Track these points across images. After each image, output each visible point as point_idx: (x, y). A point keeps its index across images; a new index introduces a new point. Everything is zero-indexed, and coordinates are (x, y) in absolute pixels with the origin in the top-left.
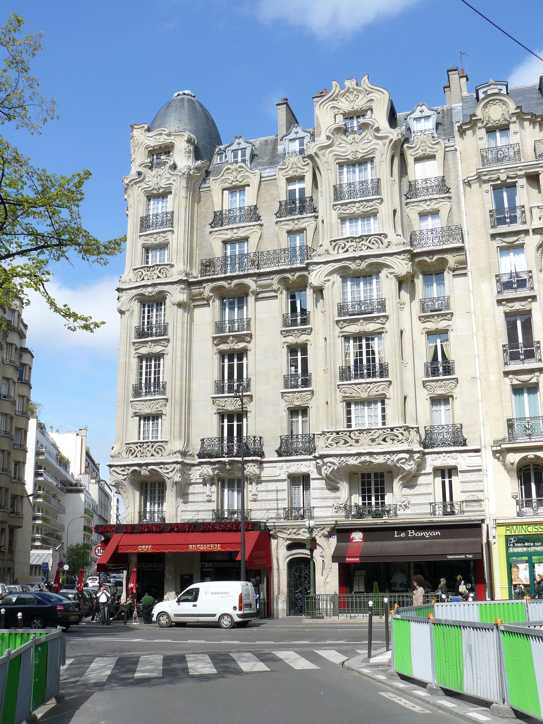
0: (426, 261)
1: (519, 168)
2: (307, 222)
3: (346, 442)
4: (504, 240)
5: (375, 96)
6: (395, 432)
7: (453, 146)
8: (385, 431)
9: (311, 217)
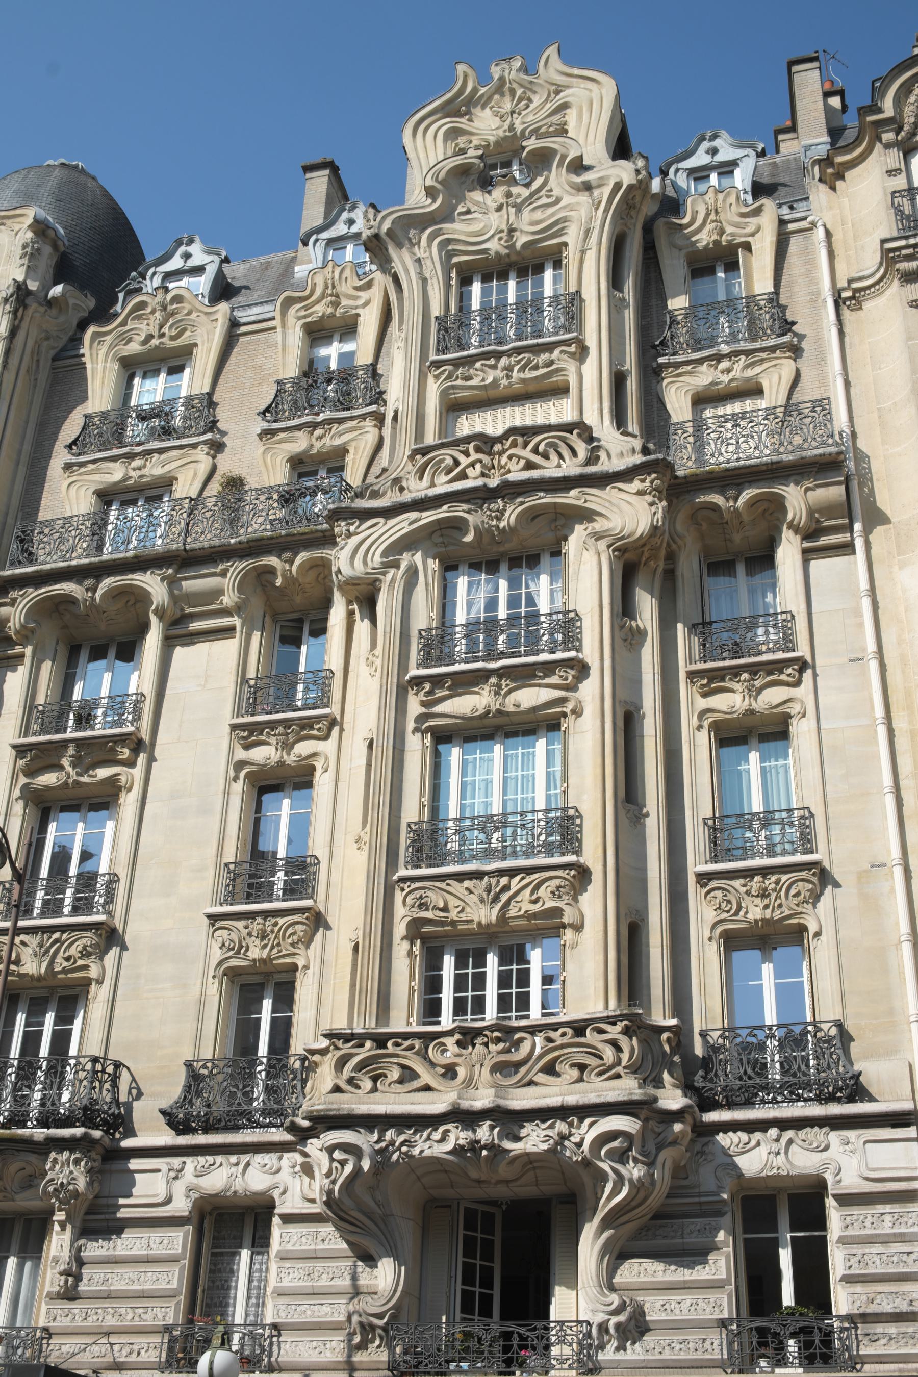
0: (715, 508)
2: (351, 430)
3: (408, 1074)
5: (577, 93)
6: (590, 1037)
7: (805, 218)
8: (552, 1034)
9: (363, 417)
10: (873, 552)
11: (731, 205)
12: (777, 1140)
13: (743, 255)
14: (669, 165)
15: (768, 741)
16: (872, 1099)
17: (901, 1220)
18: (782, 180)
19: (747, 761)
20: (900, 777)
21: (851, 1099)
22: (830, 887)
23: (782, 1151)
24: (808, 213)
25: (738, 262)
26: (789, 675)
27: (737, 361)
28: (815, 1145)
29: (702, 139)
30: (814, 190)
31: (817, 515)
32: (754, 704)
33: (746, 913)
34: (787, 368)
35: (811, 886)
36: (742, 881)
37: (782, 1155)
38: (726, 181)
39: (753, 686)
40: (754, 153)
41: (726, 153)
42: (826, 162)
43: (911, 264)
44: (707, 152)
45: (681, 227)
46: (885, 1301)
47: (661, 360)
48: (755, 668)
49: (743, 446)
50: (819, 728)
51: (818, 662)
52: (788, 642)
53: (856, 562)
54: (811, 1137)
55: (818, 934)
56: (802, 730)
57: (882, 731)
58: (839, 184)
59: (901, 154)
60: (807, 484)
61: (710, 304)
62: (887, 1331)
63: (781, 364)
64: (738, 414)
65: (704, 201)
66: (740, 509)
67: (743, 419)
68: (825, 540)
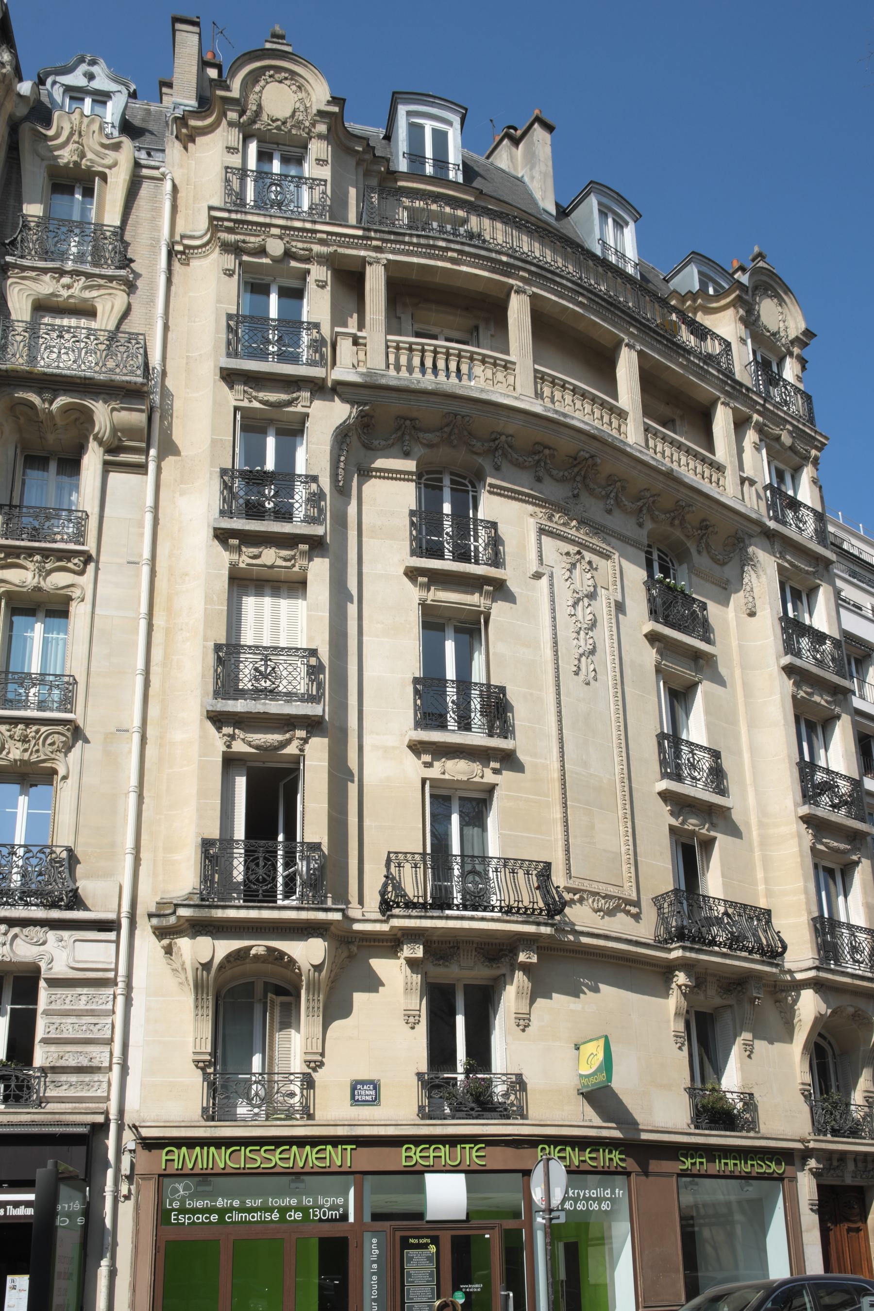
0: (31, 405)
1: (319, 235)
4: (261, 395)
7: (158, 168)
10: (163, 476)
11: (94, 132)
12: (5, 934)
13: (99, 185)
14: (48, 74)
15: (54, 617)
16: (87, 909)
17: (93, 1000)
18: (150, 128)
19: (33, 629)
20: (152, 664)
21: (69, 907)
22: (80, 742)
23: (8, 943)
24: (162, 164)
25: (93, 189)
26: (75, 564)
27: (78, 281)
28: (35, 940)
29: (82, 60)
30: (170, 144)
31: (119, 434)
32: (42, 583)
33: (8, 753)
34: (120, 299)
35: (64, 739)
36: (7, 727)
37: (8, 946)
38: (98, 109)
39: (44, 568)
40: (126, 92)
41: (102, 83)
42: (182, 121)
43: (230, 236)
44: (85, 75)
45: (46, 138)
46: (72, 1057)
47: (8, 259)
48: (46, 553)
49: (64, 357)
50: (93, 612)
51: (102, 558)
52: (80, 536)
53: (147, 482)
54: (33, 934)
55: (65, 778)
56: (79, 612)
57: (143, 625)
58: (190, 145)
59: (241, 136)
60: (114, 404)
61: (62, 220)
62: (69, 1079)
63: (116, 295)
64: (63, 326)
65: (70, 119)
66: (54, 411)
67: (68, 332)
68: (123, 457)
